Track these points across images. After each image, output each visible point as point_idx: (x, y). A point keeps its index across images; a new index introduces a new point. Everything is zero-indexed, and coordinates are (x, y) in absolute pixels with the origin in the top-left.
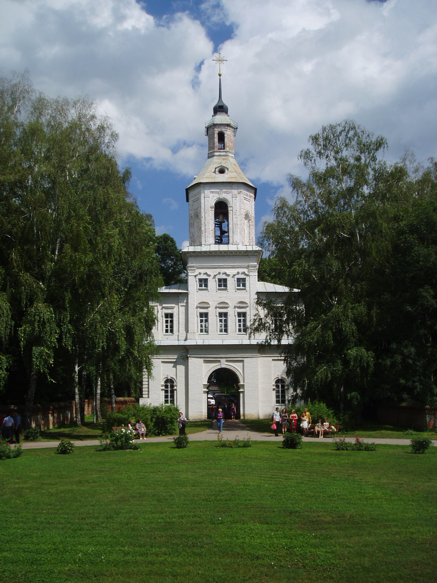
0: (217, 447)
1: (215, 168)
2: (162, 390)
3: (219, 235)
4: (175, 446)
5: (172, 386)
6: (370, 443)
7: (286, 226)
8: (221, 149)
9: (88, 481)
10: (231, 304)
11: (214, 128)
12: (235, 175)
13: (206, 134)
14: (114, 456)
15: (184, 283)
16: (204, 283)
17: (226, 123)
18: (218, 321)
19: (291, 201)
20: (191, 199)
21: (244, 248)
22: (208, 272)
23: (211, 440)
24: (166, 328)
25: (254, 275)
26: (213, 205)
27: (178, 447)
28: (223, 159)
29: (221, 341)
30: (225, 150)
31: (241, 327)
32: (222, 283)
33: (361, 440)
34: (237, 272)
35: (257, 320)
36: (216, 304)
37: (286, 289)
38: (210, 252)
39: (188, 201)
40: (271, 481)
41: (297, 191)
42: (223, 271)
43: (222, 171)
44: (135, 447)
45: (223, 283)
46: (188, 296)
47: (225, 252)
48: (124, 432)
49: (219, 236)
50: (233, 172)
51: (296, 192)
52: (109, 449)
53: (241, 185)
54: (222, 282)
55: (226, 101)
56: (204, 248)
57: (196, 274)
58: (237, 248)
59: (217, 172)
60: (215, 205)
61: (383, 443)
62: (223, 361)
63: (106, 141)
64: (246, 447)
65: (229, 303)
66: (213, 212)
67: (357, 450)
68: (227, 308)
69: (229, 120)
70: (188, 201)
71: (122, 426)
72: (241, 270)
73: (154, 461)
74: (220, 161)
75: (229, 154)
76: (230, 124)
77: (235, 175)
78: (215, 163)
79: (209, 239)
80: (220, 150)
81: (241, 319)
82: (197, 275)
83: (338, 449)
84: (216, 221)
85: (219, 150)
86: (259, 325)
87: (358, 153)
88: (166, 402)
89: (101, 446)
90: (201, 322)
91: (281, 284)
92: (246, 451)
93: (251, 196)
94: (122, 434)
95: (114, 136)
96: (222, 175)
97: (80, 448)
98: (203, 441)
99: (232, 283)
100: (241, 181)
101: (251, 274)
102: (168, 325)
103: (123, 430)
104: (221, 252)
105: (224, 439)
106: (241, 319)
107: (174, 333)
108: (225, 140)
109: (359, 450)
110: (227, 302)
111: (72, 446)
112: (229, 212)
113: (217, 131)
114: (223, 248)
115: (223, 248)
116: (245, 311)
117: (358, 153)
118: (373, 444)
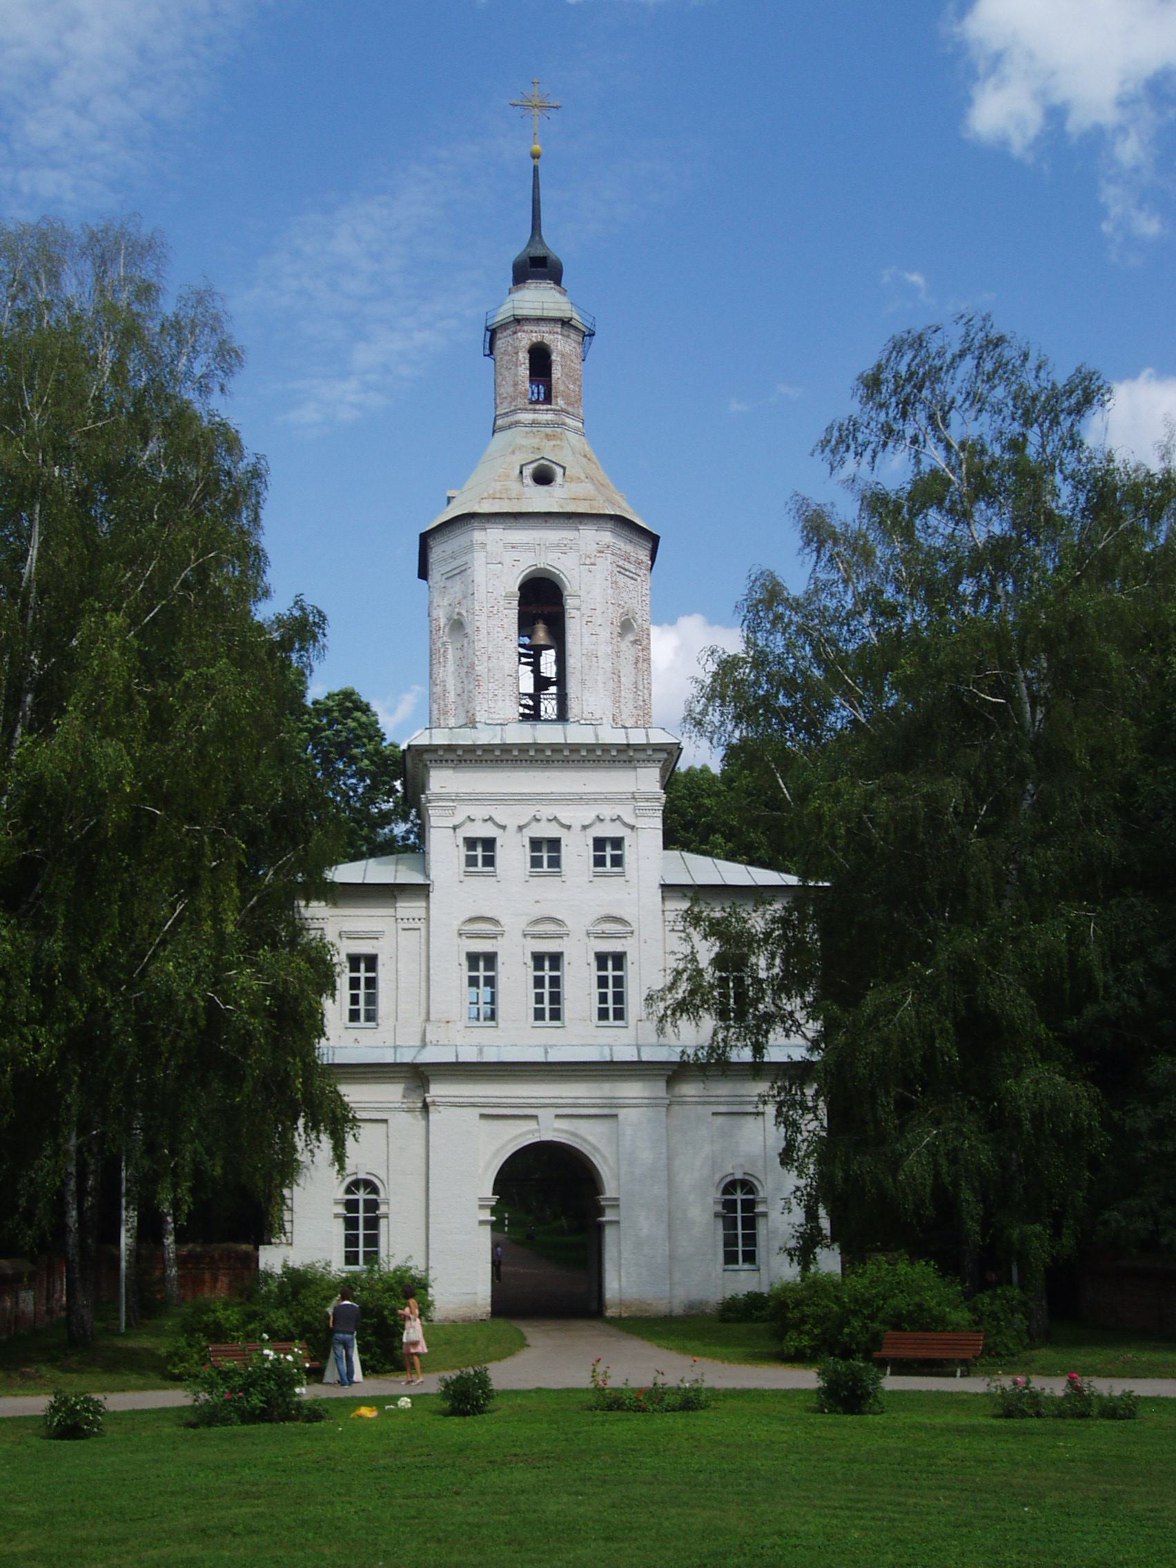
0: (590, 1409)
1: (522, 466)
2: (337, 1216)
3: (531, 690)
4: (446, 1405)
6: (1117, 1393)
7: (780, 661)
8: (537, 402)
9: (203, 1531)
10: (578, 923)
11: (515, 333)
12: (587, 488)
13: (487, 352)
14: (253, 1444)
15: (416, 847)
17: (558, 314)
19: (796, 584)
20: (435, 572)
21: (618, 737)
22: (500, 813)
23: (560, 1387)
24: (537, 1002)
25: (653, 826)
26: (515, 589)
27: (454, 1412)
28: (548, 437)
29: (542, 1050)
30: (553, 407)
31: (542, 1002)
33: (1083, 1382)
34: (593, 816)
35: (685, 976)
36: (522, 924)
37: (792, 880)
38: (506, 748)
39: (423, 573)
40: (861, 1518)
41: (818, 550)
42: (546, 811)
43: (543, 477)
44: (314, 1414)
46: (428, 896)
47: (556, 748)
48: (271, 1358)
49: (530, 696)
50: (579, 480)
51: (814, 554)
52: (226, 1421)
53: (610, 525)
54: (608, 849)
55: (556, 244)
58: (597, 736)
59: (528, 480)
60: (519, 589)
61: (1149, 1395)
62: (545, 1115)
63: (198, 370)
64: (692, 1409)
66: (513, 614)
67: (1054, 1416)
68: (560, 937)
69: (568, 306)
70: (423, 573)
71: (263, 1340)
72: (607, 811)
73: (408, 1460)
74: (534, 441)
75: (568, 421)
76: (571, 319)
77: (587, 488)
78: (521, 447)
79: (500, 703)
80: (538, 407)
81: (359, 978)
83: (1008, 1414)
84: (520, 646)
85: (531, 407)
86: (692, 993)
87: (1016, 427)
88: (351, 1258)
89: (193, 1408)
91: (730, 857)
92: (700, 1422)
93: (639, 563)
94: (267, 1365)
95: (228, 357)
96: (545, 488)
97: (118, 1417)
98: (530, 1391)
99: (576, 852)
100: (608, 512)
101: (639, 823)
102: (606, 994)
103: (266, 1352)
104: (540, 748)
105: (616, 1381)
106: (359, 978)
107: (380, 1021)
108: (553, 371)
109: (1083, 1415)
110: (558, 917)
111: (97, 1408)
112: (567, 615)
113: (527, 337)
114: (548, 734)
116: (559, 950)
117: (1016, 427)
118: (1129, 1395)
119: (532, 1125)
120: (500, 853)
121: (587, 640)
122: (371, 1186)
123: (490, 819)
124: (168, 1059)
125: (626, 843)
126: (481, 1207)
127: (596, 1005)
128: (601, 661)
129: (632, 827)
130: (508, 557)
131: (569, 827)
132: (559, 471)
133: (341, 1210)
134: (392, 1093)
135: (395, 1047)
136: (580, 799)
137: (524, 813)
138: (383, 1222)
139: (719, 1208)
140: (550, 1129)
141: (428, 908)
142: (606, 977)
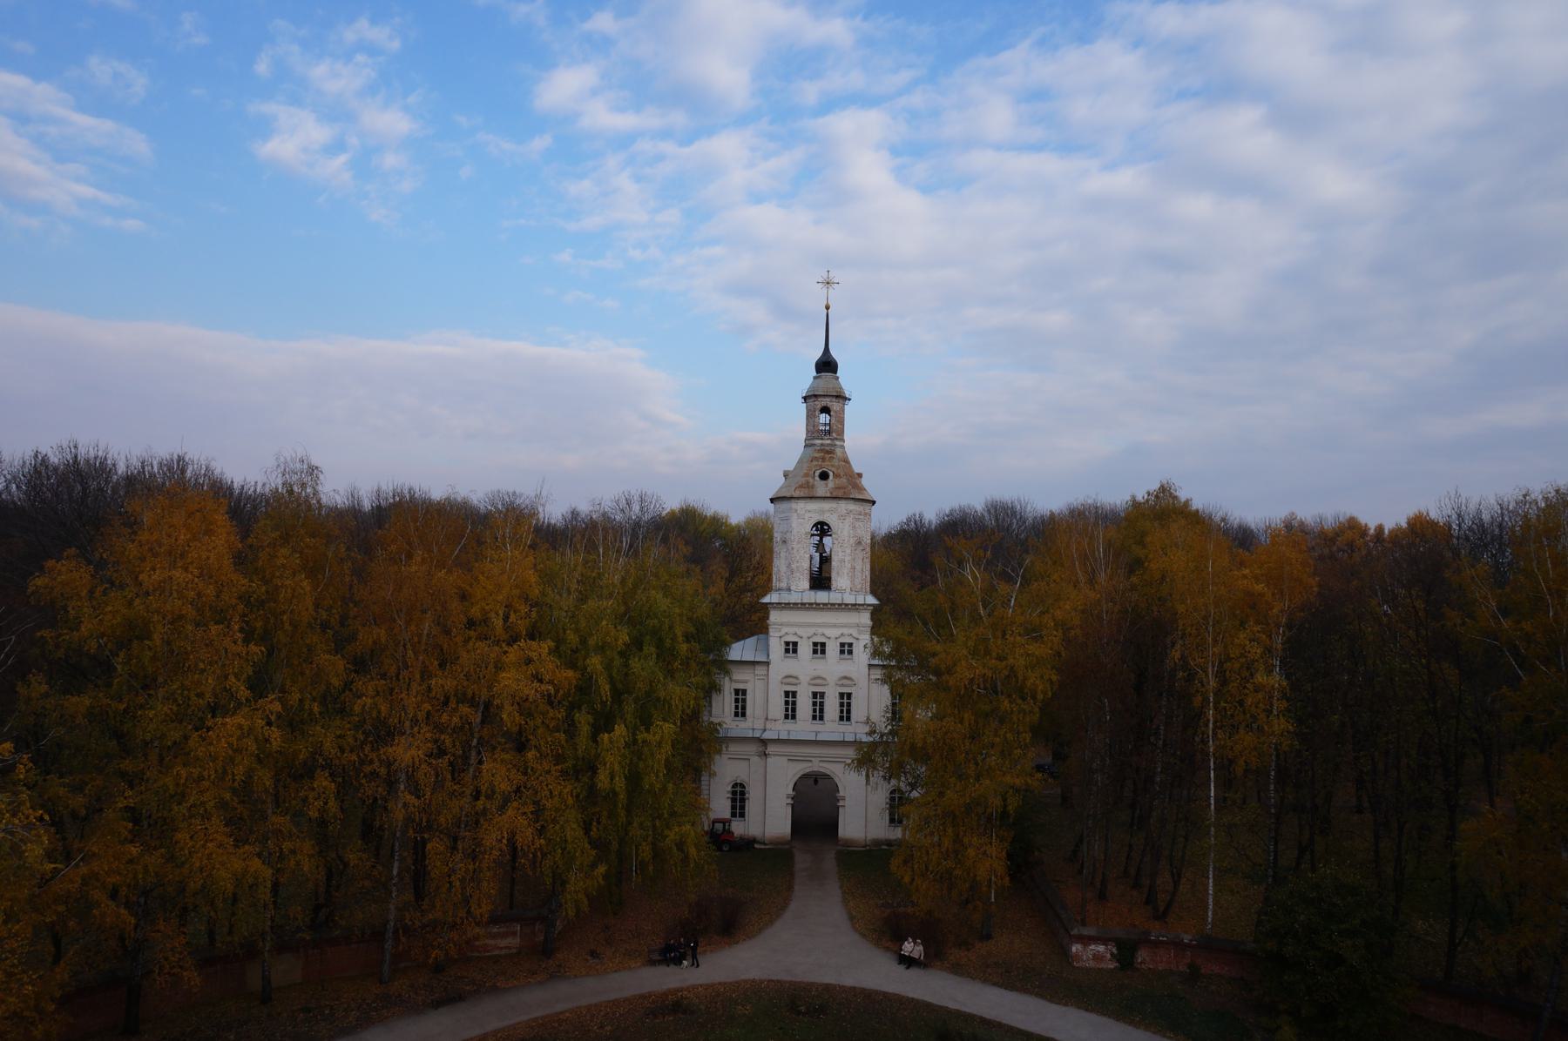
5: (743, 793)
10: (804, 679)
16: (791, 648)
18: (733, 700)
22: (800, 631)
32: (791, 647)
36: (808, 679)
42: (820, 630)
45: (819, 649)
54: (846, 646)
56: (794, 598)
57: (781, 634)
58: (843, 599)
59: (817, 478)
65: (828, 679)
68: (796, 685)
72: (846, 631)
82: (784, 636)
90: (736, 702)
96: (825, 482)
99: (832, 649)
115: (822, 596)
119: (810, 764)
120: (799, 648)
121: (840, 554)
122: (742, 786)
123: (796, 634)
124: (534, 838)
125: (854, 645)
126: (788, 797)
127: (811, 713)
128: (846, 563)
129: (857, 639)
130: (807, 515)
131: (829, 638)
132: (831, 474)
133: (730, 795)
134: (753, 749)
135: (753, 729)
136: (835, 626)
137: (811, 631)
138: (747, 801)
139: (888, 800)
140: (817, 766)
141: (768, 670)
142: (843, 703)
